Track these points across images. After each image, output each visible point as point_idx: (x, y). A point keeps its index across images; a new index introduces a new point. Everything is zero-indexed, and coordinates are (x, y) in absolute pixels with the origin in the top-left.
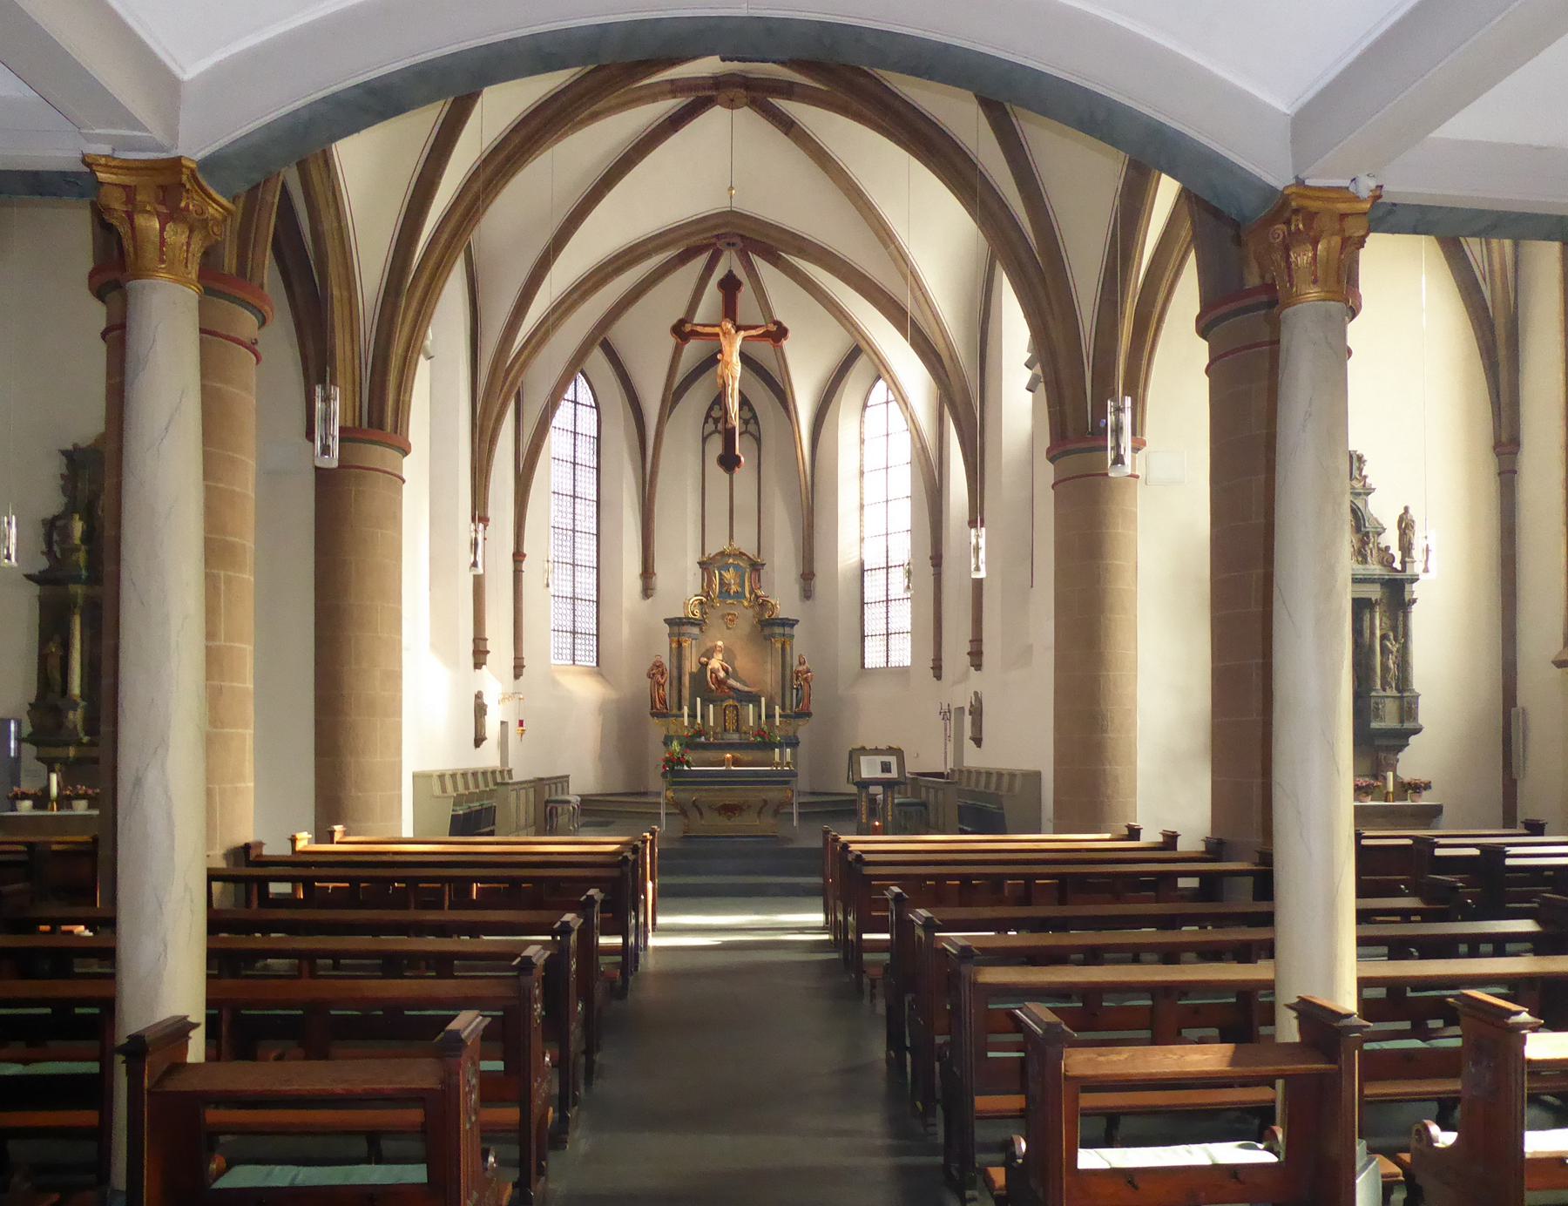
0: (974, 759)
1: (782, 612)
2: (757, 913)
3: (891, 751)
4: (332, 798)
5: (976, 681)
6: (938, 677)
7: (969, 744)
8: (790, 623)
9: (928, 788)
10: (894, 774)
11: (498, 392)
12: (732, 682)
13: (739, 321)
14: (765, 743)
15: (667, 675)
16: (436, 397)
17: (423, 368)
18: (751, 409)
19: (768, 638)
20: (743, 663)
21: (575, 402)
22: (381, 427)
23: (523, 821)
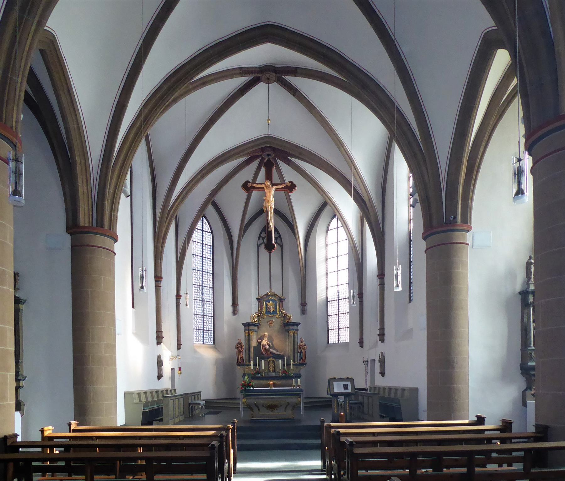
0: (380, 382)
1: (293, 319)
2: (287, 460)
3: (348, 379)
4: (82, 407)
6: (362, 346)
7: (378, 376)
8: (297, 324)
9: (363, 396)
10: (350, 390)
11: (165, 217)
13: (273, 182)
14: (286, 376)
15: (244, 348)
16: (132, 216)
17: (124, 203)
18: (279, 233)
19: (287, 331)
22: (102, 226)
23: (177, 414)
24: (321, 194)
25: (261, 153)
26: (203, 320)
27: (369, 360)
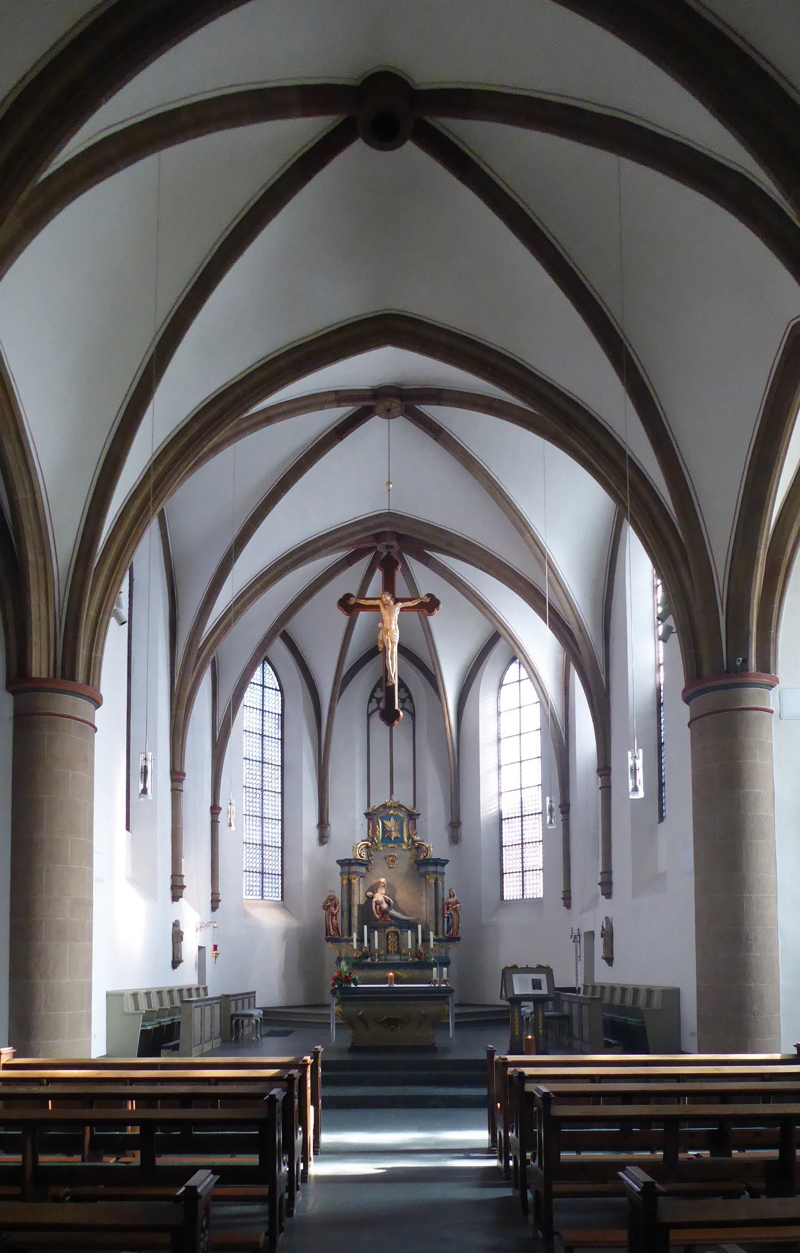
0: (604, 975)
1: (434, 854)
2: (420, 1129)
3: (540, 969)
5: (605, 908)
9: (571, 1004)
10: (544, 991)
12: (393, 912)
14: (422, 963)
15: (339, 907)
16: (129, 659)
18: (407, 690)
19: (423, 875)
20: (402, 896)
21: (263, 686)
22: (73, 677)
23: (207, 1034)
24: (488, 618)
25: (374, 544)
26: (262, 854)
27: (582, 932)
